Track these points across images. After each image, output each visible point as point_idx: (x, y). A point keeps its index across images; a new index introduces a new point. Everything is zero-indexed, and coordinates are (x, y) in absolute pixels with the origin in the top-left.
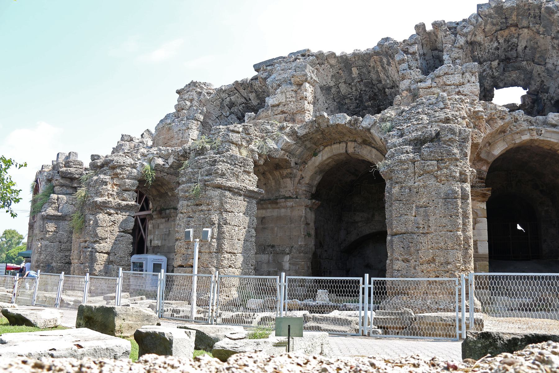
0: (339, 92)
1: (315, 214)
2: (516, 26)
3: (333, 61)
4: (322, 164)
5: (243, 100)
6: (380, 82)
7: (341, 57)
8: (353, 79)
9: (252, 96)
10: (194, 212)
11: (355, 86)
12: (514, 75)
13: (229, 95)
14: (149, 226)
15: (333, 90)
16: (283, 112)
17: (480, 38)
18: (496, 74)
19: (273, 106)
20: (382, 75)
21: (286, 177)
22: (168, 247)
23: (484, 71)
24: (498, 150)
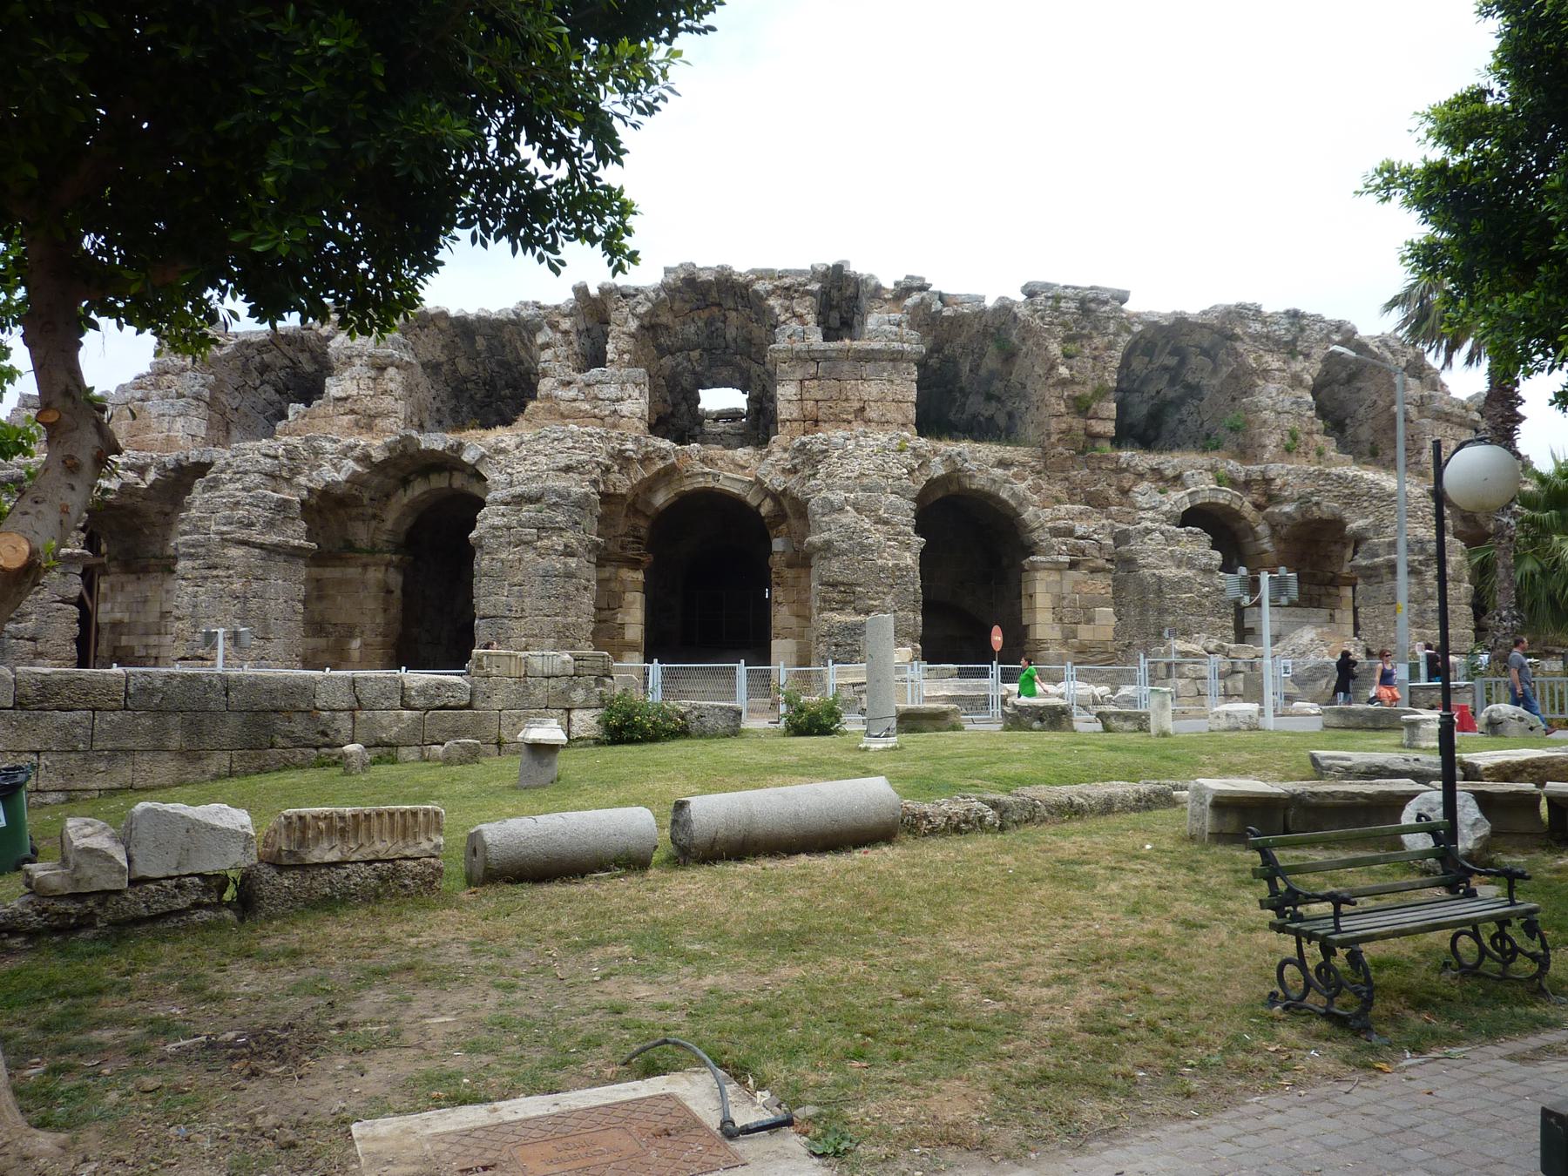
0: (456, 371)
1: (405, 576)
2: (719, 305)
3: (443, 324)
4: (413, 502)
5: (287, 362)
6: (521, 363)
7: (457, 318)
8: (479, 354)
9: (304, 358)
10: (206, 578)
11: (483, 363)
12: (726, 372)
13: (259, 352)
14: (102, 586)
15: (445, 367)
16: (352, 412)
17: (666, 318)
18: (698, 369)
19: (339, 399)
20: (523, 353)
21: (356, 518)
22: (146, 625)
23: (678, 365)
24: (661, 499)
